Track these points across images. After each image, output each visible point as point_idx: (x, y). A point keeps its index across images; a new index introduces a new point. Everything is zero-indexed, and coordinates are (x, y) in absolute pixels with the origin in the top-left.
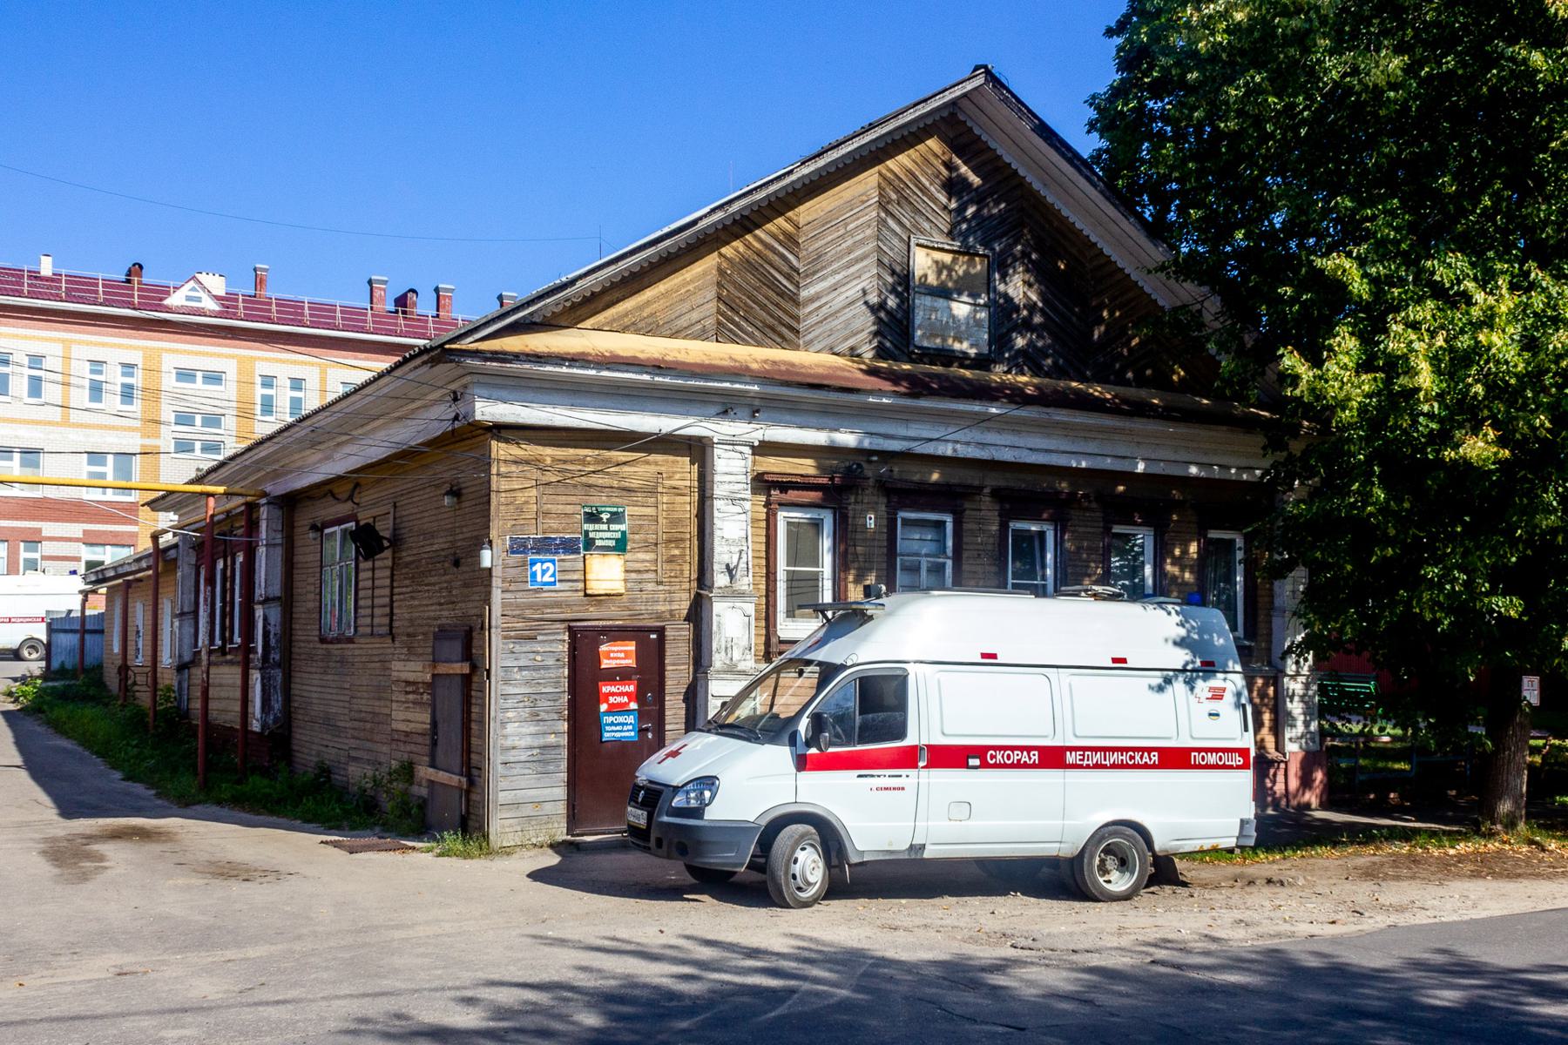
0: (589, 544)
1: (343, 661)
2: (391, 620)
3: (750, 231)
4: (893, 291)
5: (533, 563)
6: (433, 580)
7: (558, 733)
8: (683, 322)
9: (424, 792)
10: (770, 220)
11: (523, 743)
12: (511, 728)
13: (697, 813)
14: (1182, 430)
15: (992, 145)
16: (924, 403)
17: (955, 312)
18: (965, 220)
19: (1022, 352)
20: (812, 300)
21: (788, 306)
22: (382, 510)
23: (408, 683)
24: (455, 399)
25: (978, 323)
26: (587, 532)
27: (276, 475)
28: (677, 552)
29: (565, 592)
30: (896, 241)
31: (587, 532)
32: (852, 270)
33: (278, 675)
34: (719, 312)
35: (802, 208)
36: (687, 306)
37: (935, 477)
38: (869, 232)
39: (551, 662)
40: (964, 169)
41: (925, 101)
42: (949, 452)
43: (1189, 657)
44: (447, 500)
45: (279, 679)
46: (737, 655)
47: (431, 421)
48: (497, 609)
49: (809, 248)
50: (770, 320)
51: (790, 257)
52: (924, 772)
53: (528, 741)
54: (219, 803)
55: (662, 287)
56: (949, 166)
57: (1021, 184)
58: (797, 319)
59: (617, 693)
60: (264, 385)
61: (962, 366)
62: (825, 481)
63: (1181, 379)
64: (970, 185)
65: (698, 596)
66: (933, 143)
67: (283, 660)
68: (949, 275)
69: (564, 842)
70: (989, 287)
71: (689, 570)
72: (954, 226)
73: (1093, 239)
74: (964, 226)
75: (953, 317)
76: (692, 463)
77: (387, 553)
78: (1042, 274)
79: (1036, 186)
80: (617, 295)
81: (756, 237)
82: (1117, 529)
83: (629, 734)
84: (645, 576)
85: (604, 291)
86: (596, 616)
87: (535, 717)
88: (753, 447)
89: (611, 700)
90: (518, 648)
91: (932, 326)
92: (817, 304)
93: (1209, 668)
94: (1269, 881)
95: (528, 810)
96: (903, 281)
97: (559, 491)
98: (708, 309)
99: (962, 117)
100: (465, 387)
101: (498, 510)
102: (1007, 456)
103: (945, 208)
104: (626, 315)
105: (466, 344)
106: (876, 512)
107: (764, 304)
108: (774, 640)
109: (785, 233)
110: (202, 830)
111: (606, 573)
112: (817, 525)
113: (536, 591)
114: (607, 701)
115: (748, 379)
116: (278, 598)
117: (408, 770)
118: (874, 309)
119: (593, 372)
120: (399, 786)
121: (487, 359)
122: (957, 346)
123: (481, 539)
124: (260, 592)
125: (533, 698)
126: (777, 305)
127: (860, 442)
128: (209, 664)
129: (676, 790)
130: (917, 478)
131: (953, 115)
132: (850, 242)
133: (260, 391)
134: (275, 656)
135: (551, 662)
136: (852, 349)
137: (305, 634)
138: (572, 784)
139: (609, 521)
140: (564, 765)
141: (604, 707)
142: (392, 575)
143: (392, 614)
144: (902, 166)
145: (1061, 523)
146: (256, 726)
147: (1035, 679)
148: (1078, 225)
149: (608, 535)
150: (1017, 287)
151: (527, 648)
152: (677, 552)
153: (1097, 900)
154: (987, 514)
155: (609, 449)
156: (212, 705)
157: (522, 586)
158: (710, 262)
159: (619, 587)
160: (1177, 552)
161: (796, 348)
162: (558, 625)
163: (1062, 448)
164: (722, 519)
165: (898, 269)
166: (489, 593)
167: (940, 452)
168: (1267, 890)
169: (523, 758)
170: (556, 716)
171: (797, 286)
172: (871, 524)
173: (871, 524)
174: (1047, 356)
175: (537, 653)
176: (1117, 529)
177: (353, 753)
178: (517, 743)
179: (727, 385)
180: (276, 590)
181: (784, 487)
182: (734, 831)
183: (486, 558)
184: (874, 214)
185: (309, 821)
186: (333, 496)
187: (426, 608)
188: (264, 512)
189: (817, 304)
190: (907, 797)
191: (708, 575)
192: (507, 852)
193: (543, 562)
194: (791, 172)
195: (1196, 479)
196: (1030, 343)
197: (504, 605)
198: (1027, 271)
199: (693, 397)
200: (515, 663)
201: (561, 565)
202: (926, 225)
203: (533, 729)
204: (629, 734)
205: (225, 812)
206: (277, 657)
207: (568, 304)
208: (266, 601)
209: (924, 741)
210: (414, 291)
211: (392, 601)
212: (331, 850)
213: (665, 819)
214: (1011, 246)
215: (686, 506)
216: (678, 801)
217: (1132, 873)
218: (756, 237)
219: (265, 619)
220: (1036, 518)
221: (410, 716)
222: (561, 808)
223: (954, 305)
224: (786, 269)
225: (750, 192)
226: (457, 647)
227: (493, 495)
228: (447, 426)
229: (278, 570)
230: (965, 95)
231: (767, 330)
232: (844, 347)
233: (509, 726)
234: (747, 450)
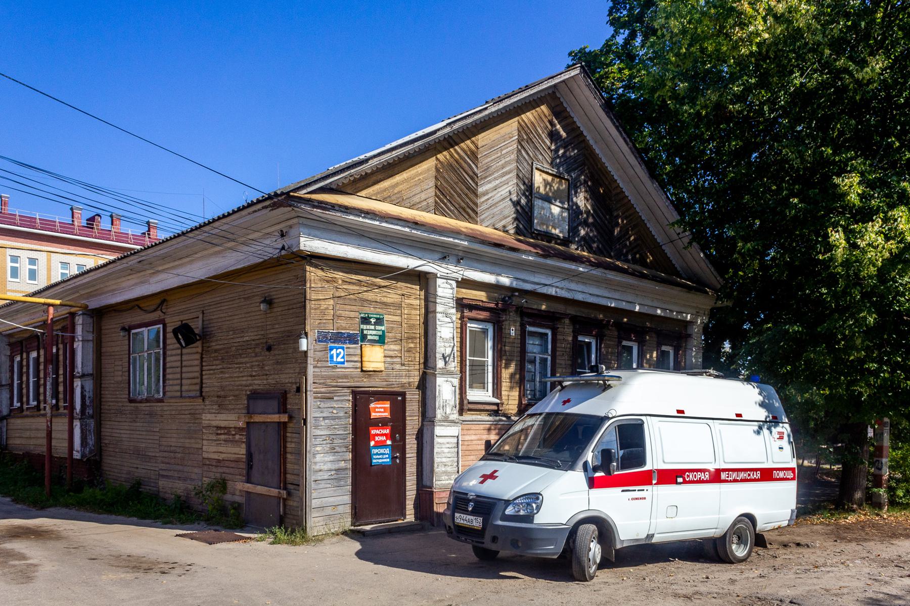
0: (364, 337)
1: (151, 414)
2: (201, 387)
3: (452, 147)
4: (524, 194)
5: (331, 349)
6: (244, 360)
7: (346, 460)
8: (416, 199)
9: (238, 499)
10: (463, 141)
11: (325, 467)
12: (319, 458)
13: (529, 518)
14: (658, 287)
15: (572, 115)
16: (549, 262)
17: (553, 211)
18: (558, 157)
19: (583, 238)
20: (484, 194)
21: (472, 196)
22: (195, 315)
23: (218, 428)
24: (282, 235)
25: (563, 218)
26: (362, 330)
27: (90, 296)
28: (412, 345)
29: (350, 368)
30: (525, 164)
31: (362, 330)
32: (504, 178)
33: (92, 423)
34: (436, 195)
35: (480, 136)
36: (418, 189)
37: (544, 307)
38: (512, 157)
39: (342, 414)
40: (558, 126)
41: (552, 77)
42: (554, 293)
43: (766, 414)
44: (262, 306)
45: (92, 425)
46: (448, 411)
47: (267, 247)
48: (310, 379)
49: (483, 162)
50: (463, 204)
51: (473, 166)
52: (655, 487)
53: (329, 466)
54: (67, 506)
55: (405, 175)
56: (551, 123)
57: (585, 141)
58: (476, 204)
59: (379, 434)
60: (12, 261)
61: (556, 243)
62: (492, 305)
63: (651, 262)
64: (561, 136)
65: (424, 373)
66: (544, 108)
67: (96, 411)
68: (550, 189)
69: (351, 530)
70: (569, 199)
71: (418, 357)
72: (553, 159)
73: (616, 177)
74: (558, 161)
75: (551, 213)
76: (421, 290)
77: (199, 344)
78: (593, 195)
79: (591, 142)
80: (380, 177)
81: (455, 150)
82: (625, 343)
83: (387, 460)
84: (395, 360)
85: (373, 173)
86: (366, 384)
87: (333, 450)
88: (457, 282)
89: (377, 438)
90: (322, 405)
91: (542, 217)
92: (486, 197)
93: (774, 421)
94: (798, 545)
95: (329, 511)
96: (529, 189)
97: (347, 302)
98: (429, 193)
99: (558, 95)
100: (291, 227)
101: (310, 313)
102: (580, 297)
103: (549, 148)
104: (385, 190)
105: (302, 193)
106: (515, 326)
107: (459, 193)
108: (465, 402)
109: (470, 150)
110: (75, 528)
111: (375, 357)
112: (485, 332)
113: (333, 367)
114: (374, 439)
115: (463, 237)
116: (92, 375)
117: (222, 485)
118: (516, 204)
119: (377, 223)
120: (215, 495)
121: (314, 207)
122: (553, 231)
123: (300, 331)
124: (79, 369)
125: (331, 438)
126: (466, 195)
127: (512, 283)
128: (52, 416)
129: (507, 503)
130: (535, 307)
131: (554, 92)
132: (503, 162)
133: (10, 265)
134: (90, 411)
135: (342, 414)
136: (504, 227)
137: (113, 398)
138: (354, 493)
139: (376, 324)
140: (349, 481)
141: (372, 443)
142: (202, 358)
143: (202, 383)
144: (529, 119)
145: (600, 338)
146: (77, 455)
147: (701, 426)
148: (609, 169)
149: (374, 332)
150: (581, 200)
151: (328, 405)
152: (412, 345)
153: (731, 563)
154: (567, 331)
155: (376, 277)
156: (54, 443)
157: (325, 364)
158: (429, 164)
159: (380, 366)
160: (648, 356)
161: (476, 223)
162: (346, 390)
163: (607, 295)
164: (440, 325)
165: (526, 181)
166: (306, 368)
167: (549, 293)
168: (796, 550)
169: (326, 477)
170: (344, 450)
171: (477, 184)
172: (513, 333)
173: (513, 333)
174: (594, 242)
175: (334, 408)
176: (625, 343)
177: (162, 473)
178: (322, 467)
179: (451, 240)
180: (89, 369)
181: (472, 307)
182: (551, 532)
183: (304, 344)
184: (515, 146)
185: (144, 518)
186: (139, 308)
187: (245, 377)
188: (79, 320)
189: (486, 197)
190: (647, 502)
191: (431, 360)
192: (318, 540)
193: (337, 349)
194: (486, 109)
195: (660, 317)
196: (587, 234)
197: (314, 376)
198: (586, 191)
199: (427, 246)
200: (321, 415)
201: (348, 350)
202: (540, 157)
203: (331, 458)
204: (387, 460)
205: (73, 512)
206: (91, 412)
207: (352, 179)
208: (83, 376)
209: (655, 468)
210: (99, 215)
211: (202, 375)
212: (188, 542)
213: (500, 523)
214: (579, 176)
215: (417, 316)
216: (510, 511)
217: (746, 545)
218: (455, 150)
219: (82, 387)
220: (589, 334)
221: (221, 449)
222: (348, 509)
223: (552, 207)
224: (471, 173)
225: (465, 118)
226: (274, 404)
227: (307, 302)
228: (275, 253)
229: (90, 356)
230: (564, 81)
231: (461, 210)
232: (500, 225)
233: (318, 456)
234: (454, 284)
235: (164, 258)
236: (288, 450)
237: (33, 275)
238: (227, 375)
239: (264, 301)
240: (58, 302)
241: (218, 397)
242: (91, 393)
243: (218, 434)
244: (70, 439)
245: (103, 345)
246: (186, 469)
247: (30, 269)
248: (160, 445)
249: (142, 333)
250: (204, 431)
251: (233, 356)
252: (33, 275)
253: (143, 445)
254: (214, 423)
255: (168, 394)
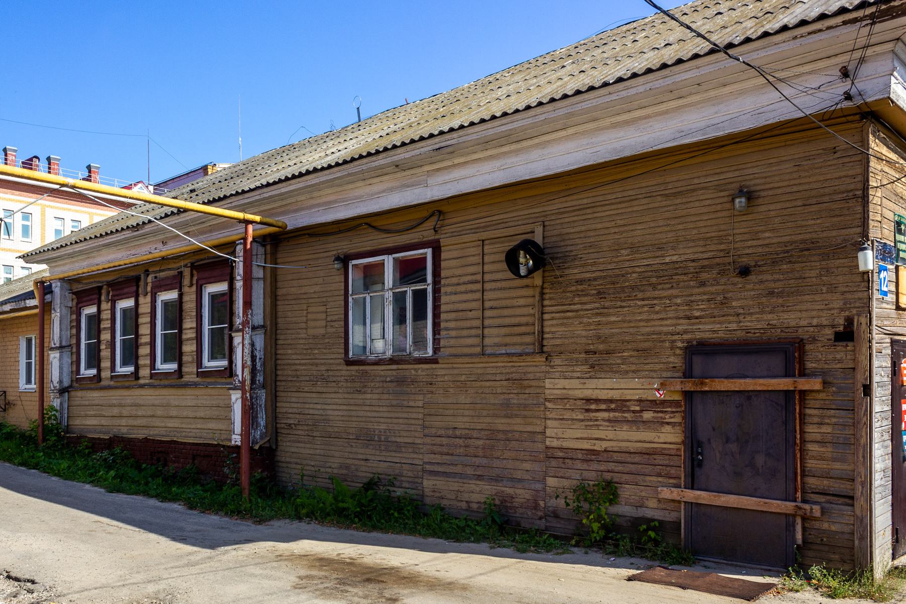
23: (588, 400)
24: (845, 74)
45: (263, 398)
116: (263, 326)
123: (861, 241)
142: (542, 294)
177: (428, 467)
226: (777, 362)
235: (486, 143)
236: (808, 437)
237: (26, 231)
238: (613, 319)
239: (741, 193)
240: (258, 218)
241: (586, 352)
242: (262, 353)
243: (588, 410)
244: (227, 418)
245: (279, 284)
246: (497, 463)
247: (23, 225)
248: (424, 427)
249: (382, 264)
250: (549, 405)
251: (633, 288)
252: (26, 231)
253: (383, 427)
254: (579, 394)
255: (444, 352)
